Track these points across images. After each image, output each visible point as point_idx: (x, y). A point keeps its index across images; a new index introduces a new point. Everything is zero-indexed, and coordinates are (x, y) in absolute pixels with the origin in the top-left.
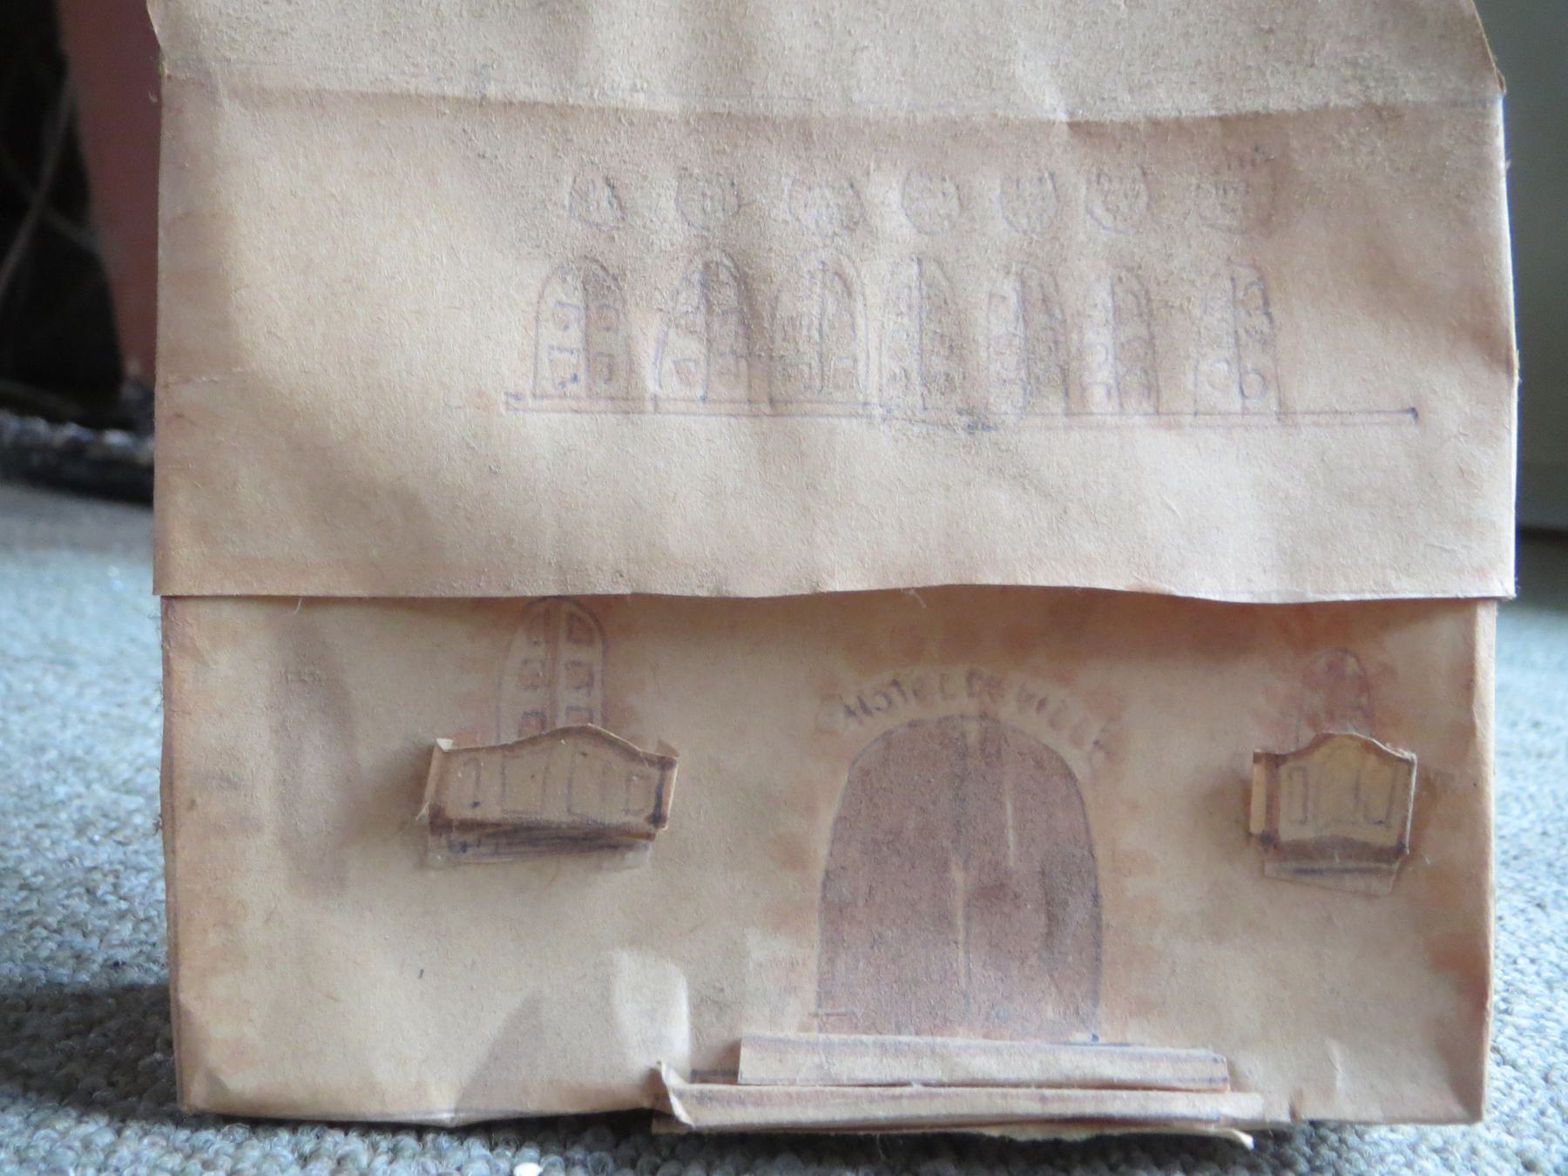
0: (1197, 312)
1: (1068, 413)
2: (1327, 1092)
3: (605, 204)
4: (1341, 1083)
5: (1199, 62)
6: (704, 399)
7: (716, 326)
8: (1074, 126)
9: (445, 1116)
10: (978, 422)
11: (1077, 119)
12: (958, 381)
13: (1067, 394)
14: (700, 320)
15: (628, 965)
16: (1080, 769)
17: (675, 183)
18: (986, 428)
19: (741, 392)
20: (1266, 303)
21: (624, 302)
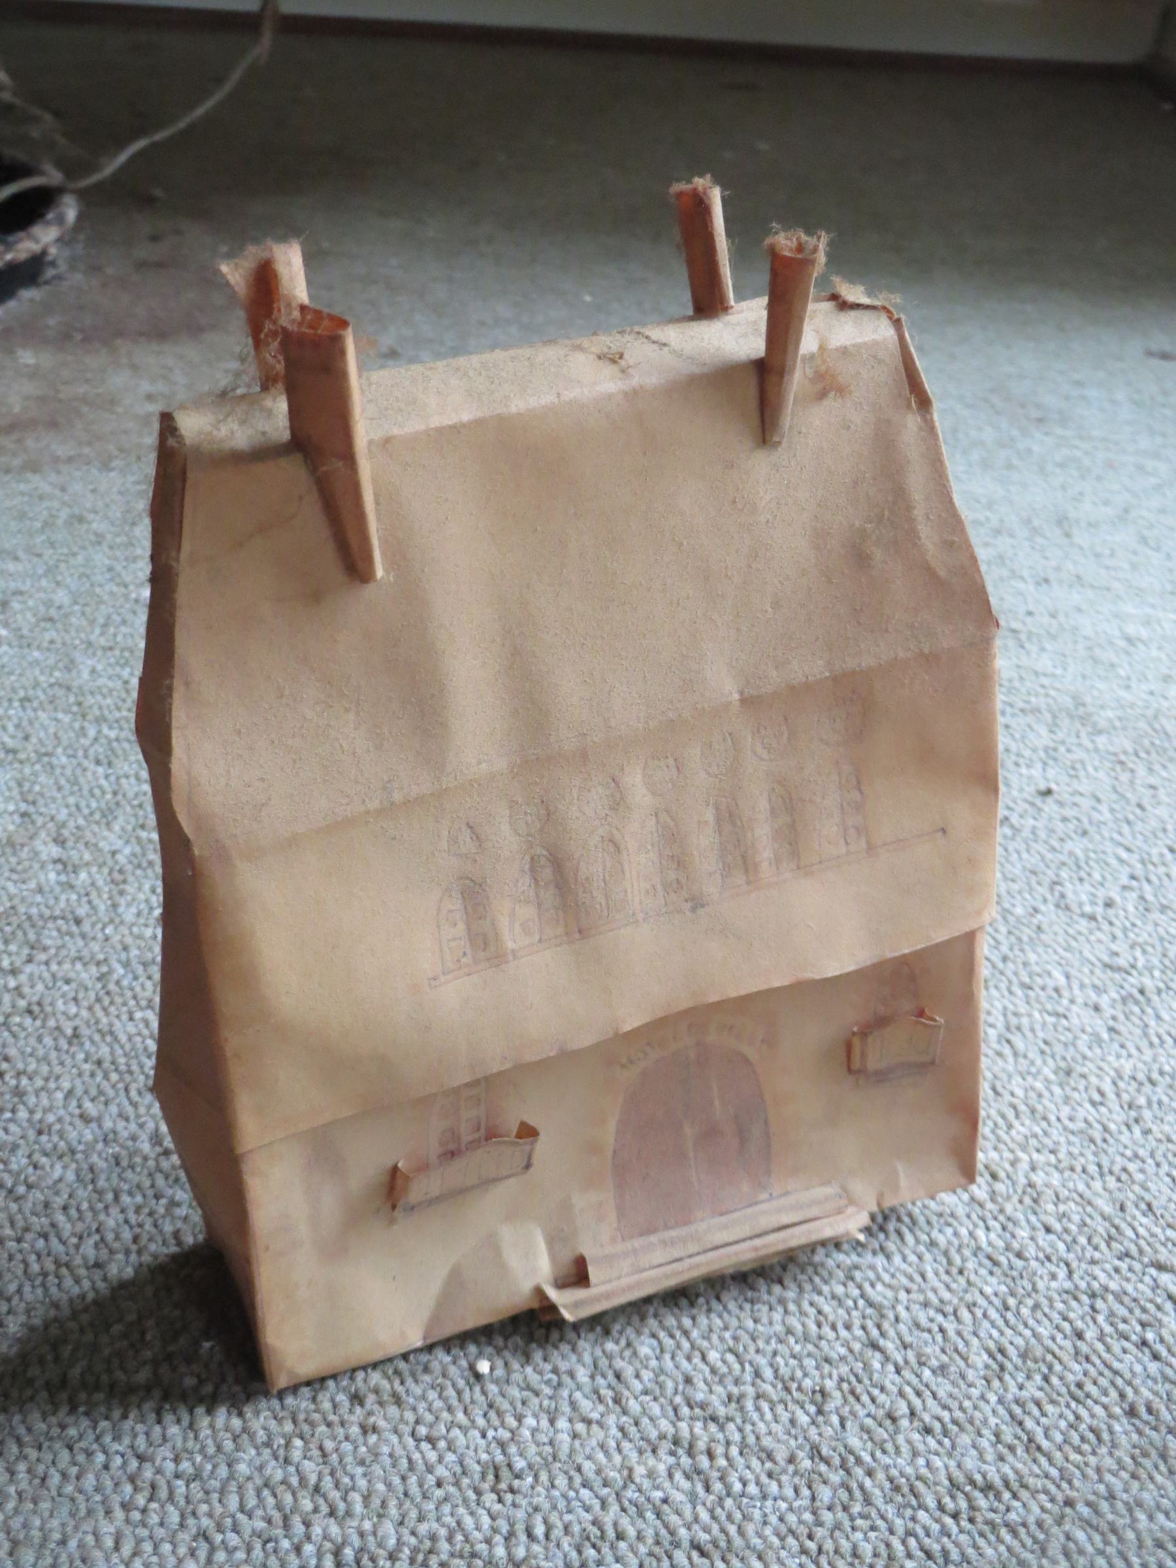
0: (818, 800)
1: (748, 883)
2: (896, 1188)
3: (468, 840)
4: (903, 1182)
5: (817, 639)
6: (540, 941)
7: (542, 893)
8: (743, 701)
9: (419, 1344)
10: (697, 903)
11: (746, 695)
12: (684, 881)
13: (746, 871)
14: (532, 893)
15: (507, 1234)
16: (750, 1052)
17: (508, 812)
18: (703, 906)
19: (560, 930)
20: (859, 782)
21: (488, 898)
